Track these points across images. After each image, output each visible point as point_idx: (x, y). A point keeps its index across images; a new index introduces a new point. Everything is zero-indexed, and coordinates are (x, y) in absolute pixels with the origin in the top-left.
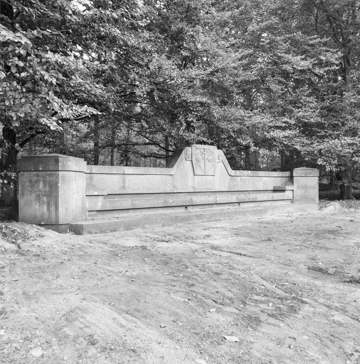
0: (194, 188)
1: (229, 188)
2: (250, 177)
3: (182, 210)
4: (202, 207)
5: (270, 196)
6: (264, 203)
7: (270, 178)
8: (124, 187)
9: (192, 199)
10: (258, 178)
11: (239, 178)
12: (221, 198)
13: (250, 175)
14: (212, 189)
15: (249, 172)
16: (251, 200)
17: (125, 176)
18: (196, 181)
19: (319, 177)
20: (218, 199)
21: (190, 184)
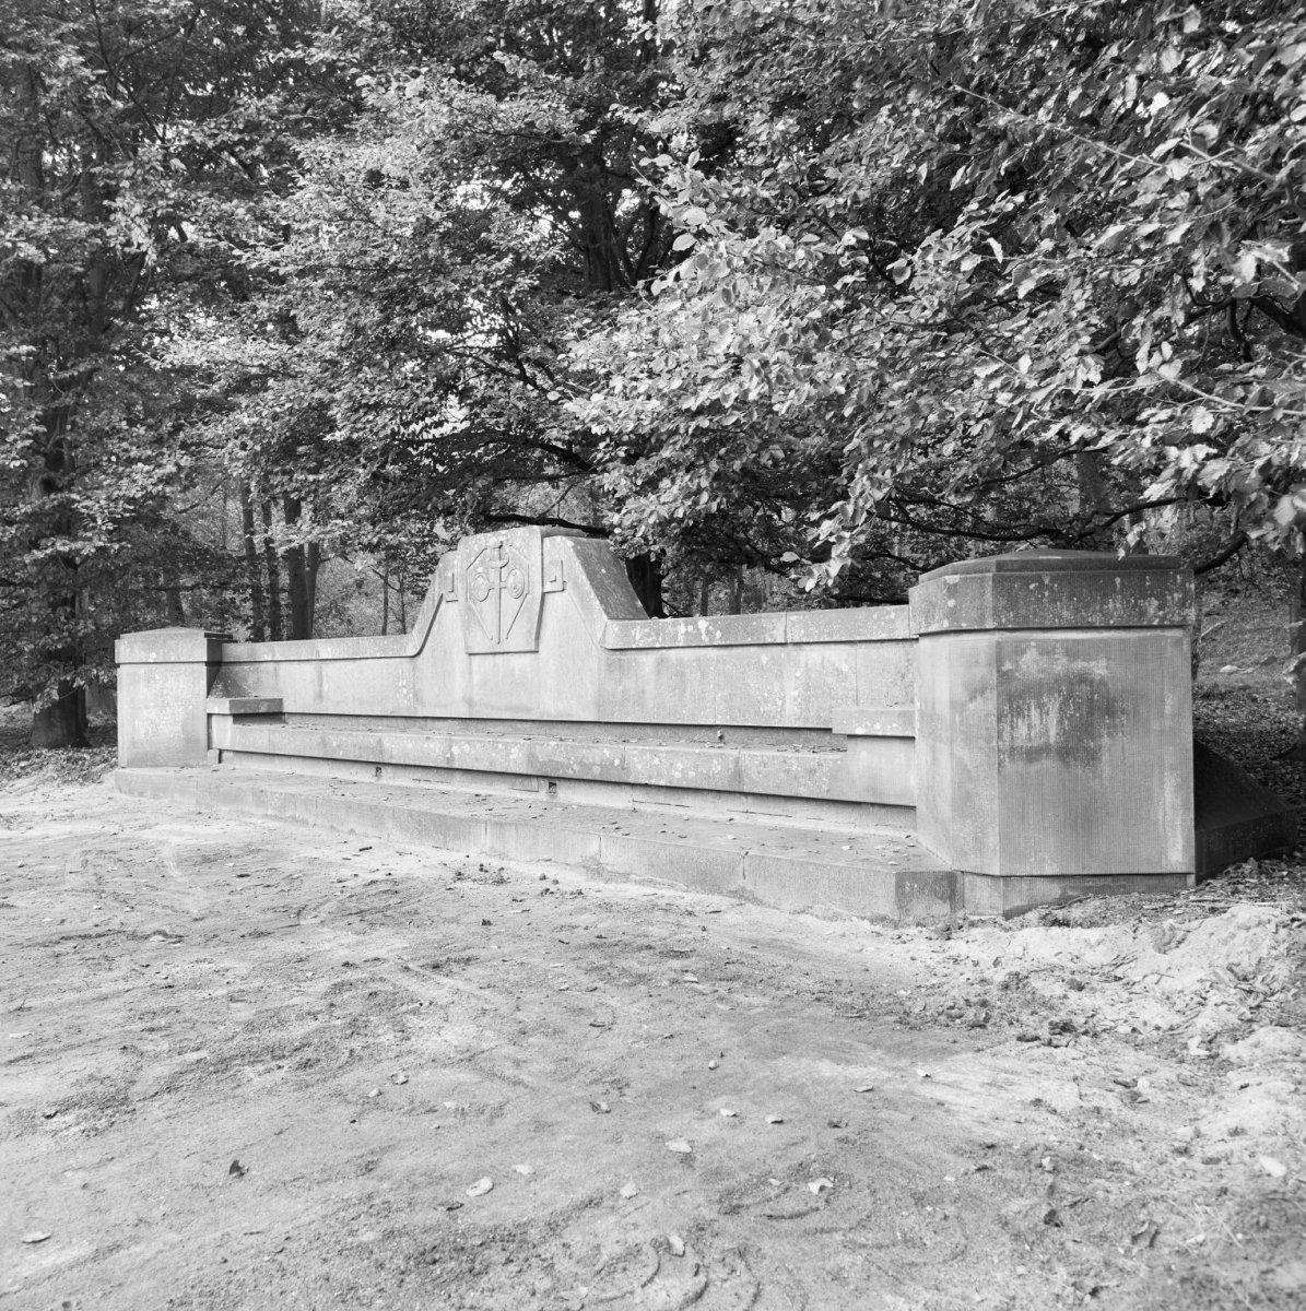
0: (470, 703)
1: (599, 706)
2: (713, 653)
3: (365, 775)
4: (419, 774)
5: (717, 767)
6: (688, 800)
7: (862, 649)
8: (320, 696)
9: (380, 742)
10: (765, 656)
11: (644, 658)
12: (467, 748)
13: (705, 639)
14: (529, 710)
15: (703, 623)
16: (596, 773)
17: (323, 665)
18: (476, 678)
19: (207, 663)
20: (455, 750)
21: (459, 687)
